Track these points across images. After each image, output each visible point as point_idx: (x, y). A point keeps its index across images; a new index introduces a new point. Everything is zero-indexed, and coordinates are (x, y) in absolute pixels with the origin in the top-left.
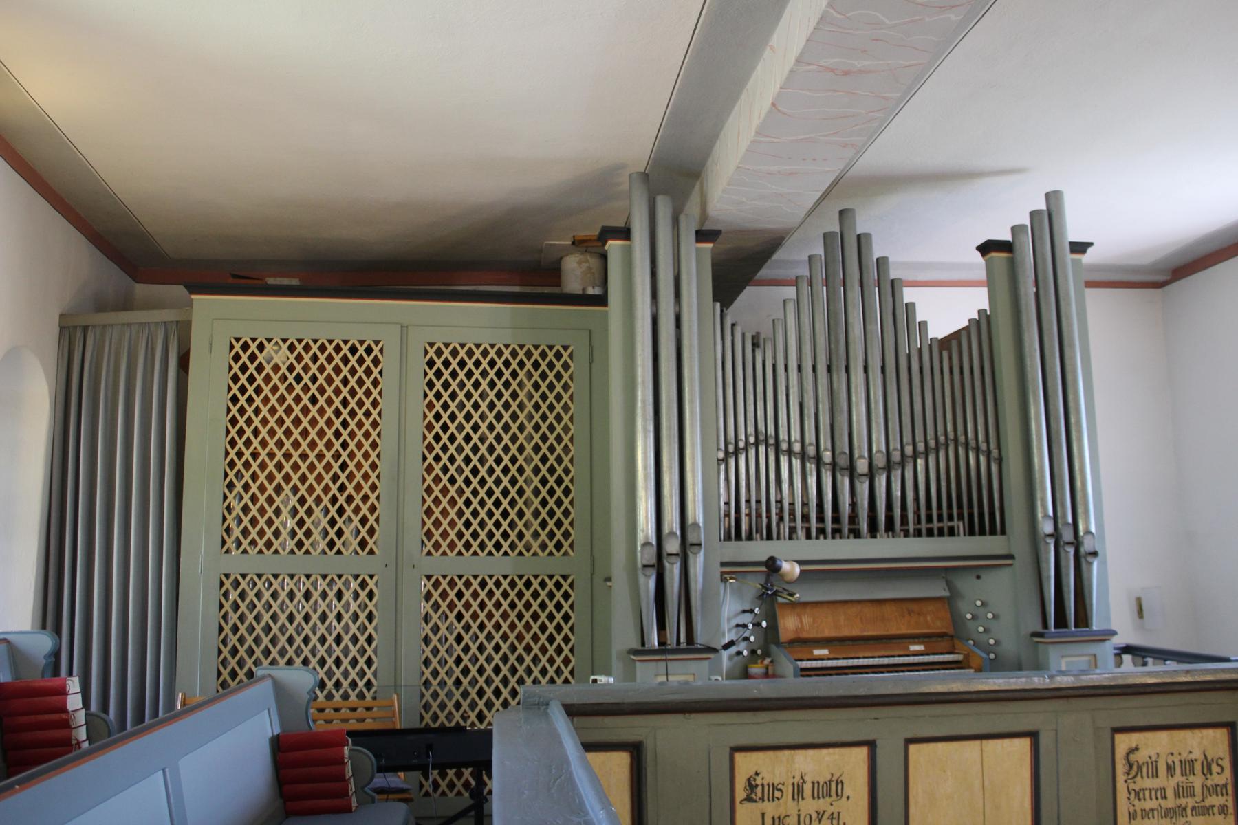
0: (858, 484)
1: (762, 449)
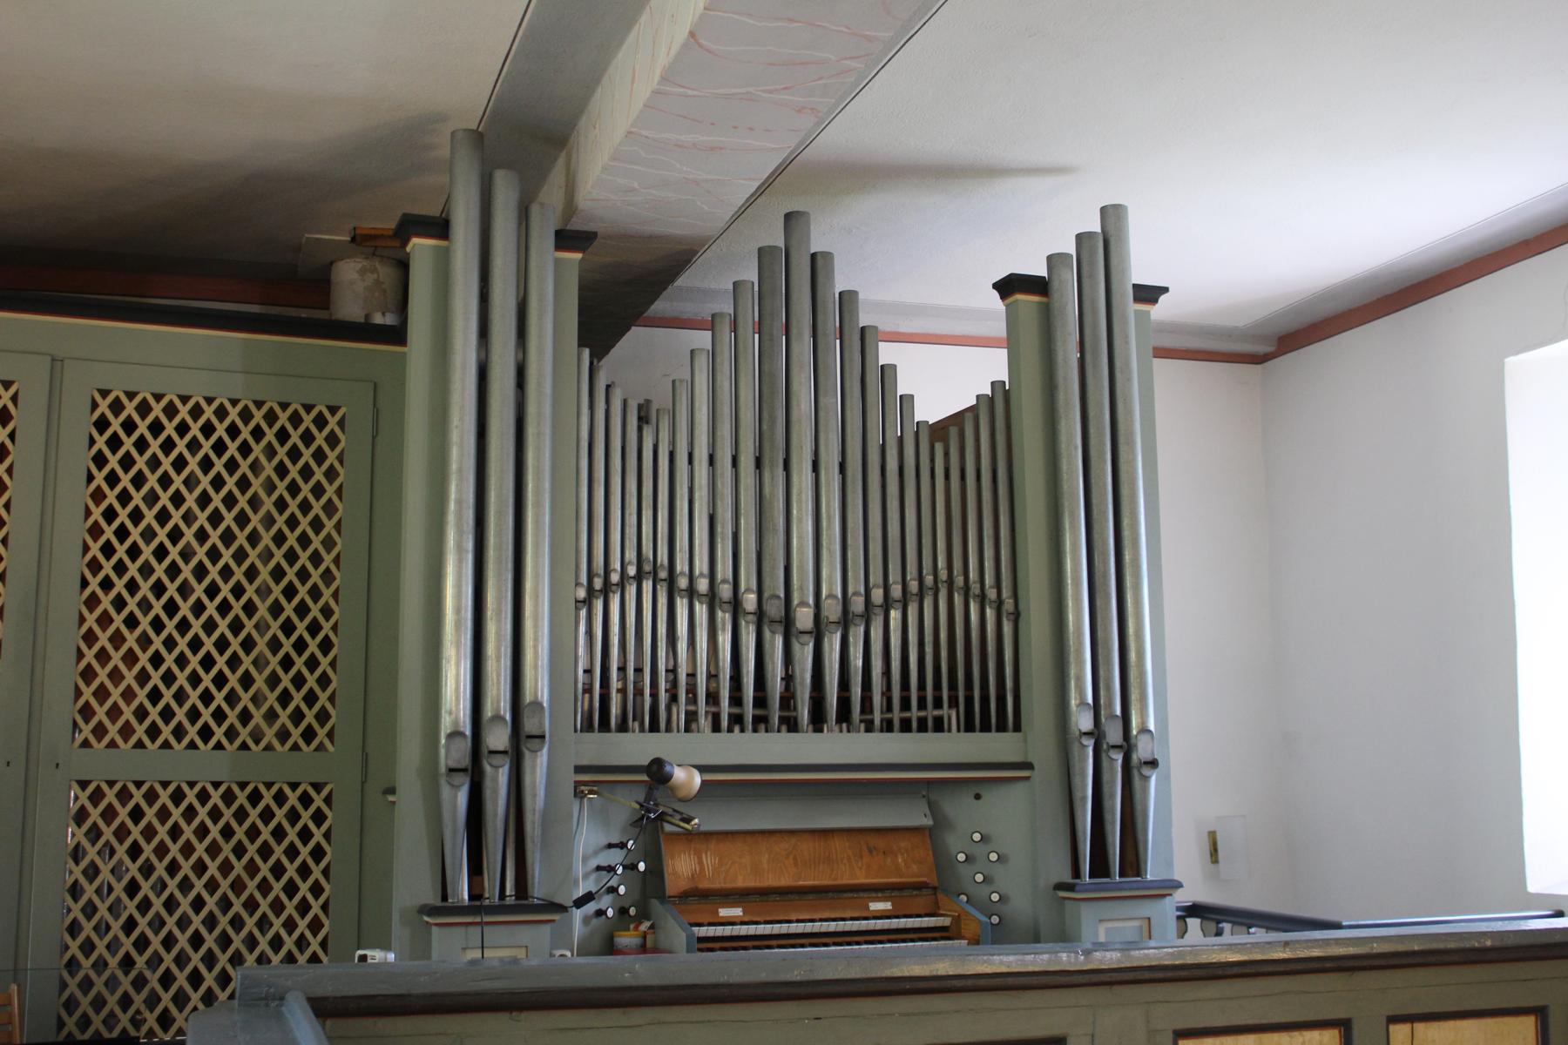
0: (796, 647)
1: (647, 586)
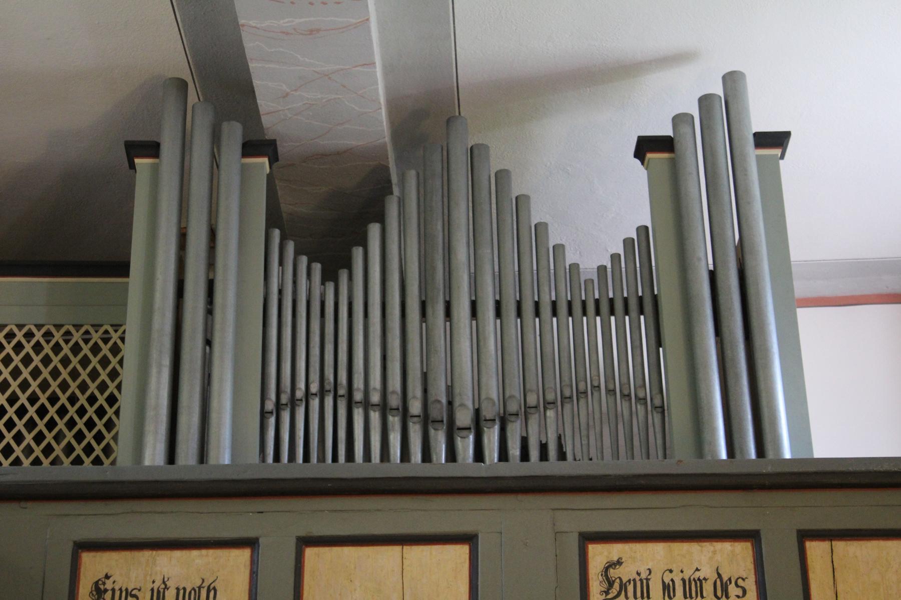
0: (459, 442)
1: (329, 401)
